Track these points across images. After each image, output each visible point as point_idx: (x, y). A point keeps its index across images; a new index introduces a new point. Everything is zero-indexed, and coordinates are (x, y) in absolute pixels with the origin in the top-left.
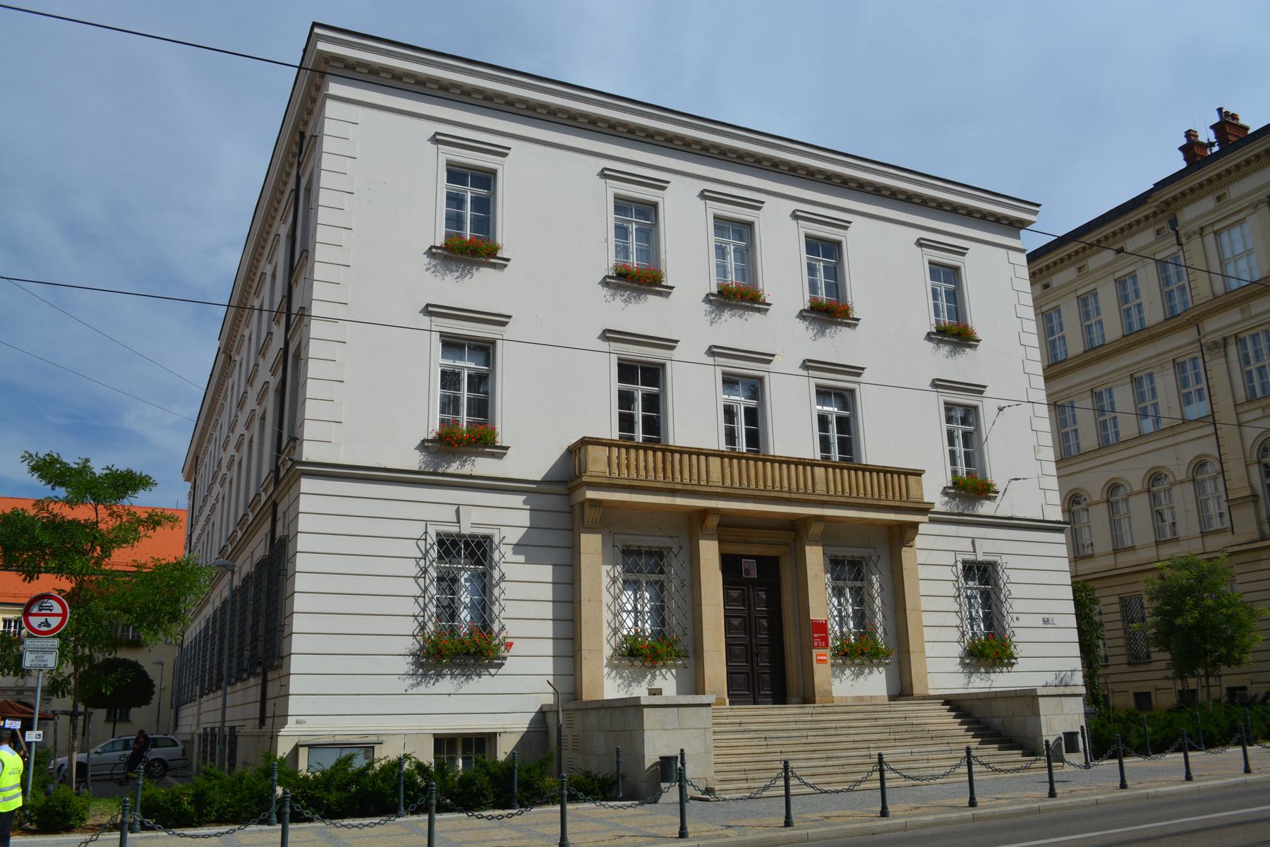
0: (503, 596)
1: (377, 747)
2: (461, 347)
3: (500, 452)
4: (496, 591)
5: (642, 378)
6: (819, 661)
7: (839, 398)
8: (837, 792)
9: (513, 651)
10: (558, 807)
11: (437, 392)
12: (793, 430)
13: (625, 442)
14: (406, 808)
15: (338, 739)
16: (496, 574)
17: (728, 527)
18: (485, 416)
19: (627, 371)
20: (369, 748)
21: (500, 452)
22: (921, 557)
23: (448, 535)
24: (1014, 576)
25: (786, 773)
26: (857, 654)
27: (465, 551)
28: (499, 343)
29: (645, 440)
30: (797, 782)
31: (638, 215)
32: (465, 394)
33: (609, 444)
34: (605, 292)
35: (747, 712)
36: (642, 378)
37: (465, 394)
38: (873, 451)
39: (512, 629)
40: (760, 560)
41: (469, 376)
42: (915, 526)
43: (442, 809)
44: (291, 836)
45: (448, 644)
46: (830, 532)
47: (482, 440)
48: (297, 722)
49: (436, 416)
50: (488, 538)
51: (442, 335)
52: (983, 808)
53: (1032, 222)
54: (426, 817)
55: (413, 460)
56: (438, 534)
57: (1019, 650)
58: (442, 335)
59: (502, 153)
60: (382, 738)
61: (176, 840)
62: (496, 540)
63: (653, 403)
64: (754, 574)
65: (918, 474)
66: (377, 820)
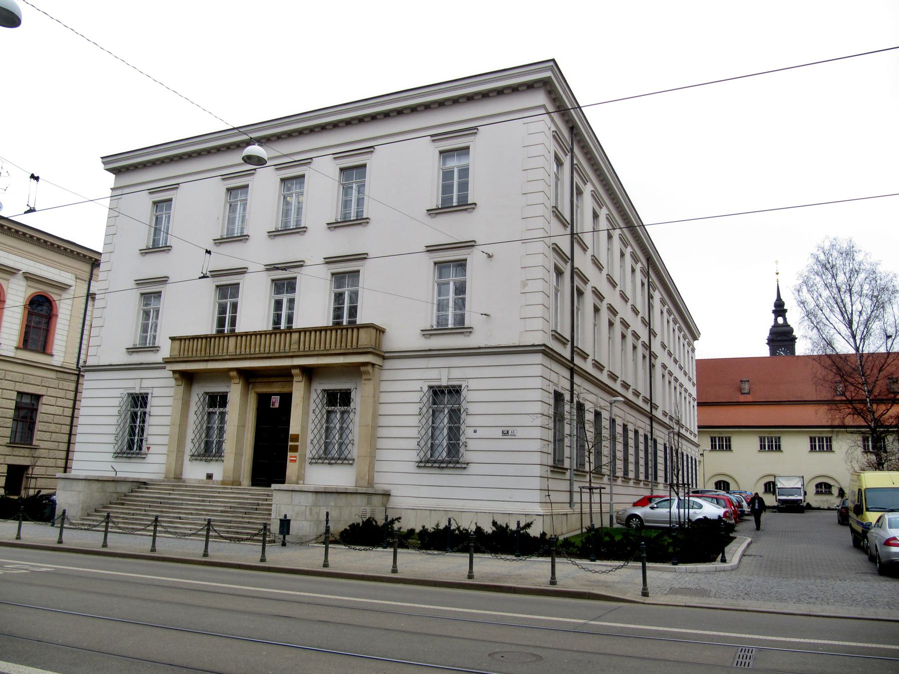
9: (151, 451)
34: (329, 232)
40: (281, 395)
64: (277, 405)
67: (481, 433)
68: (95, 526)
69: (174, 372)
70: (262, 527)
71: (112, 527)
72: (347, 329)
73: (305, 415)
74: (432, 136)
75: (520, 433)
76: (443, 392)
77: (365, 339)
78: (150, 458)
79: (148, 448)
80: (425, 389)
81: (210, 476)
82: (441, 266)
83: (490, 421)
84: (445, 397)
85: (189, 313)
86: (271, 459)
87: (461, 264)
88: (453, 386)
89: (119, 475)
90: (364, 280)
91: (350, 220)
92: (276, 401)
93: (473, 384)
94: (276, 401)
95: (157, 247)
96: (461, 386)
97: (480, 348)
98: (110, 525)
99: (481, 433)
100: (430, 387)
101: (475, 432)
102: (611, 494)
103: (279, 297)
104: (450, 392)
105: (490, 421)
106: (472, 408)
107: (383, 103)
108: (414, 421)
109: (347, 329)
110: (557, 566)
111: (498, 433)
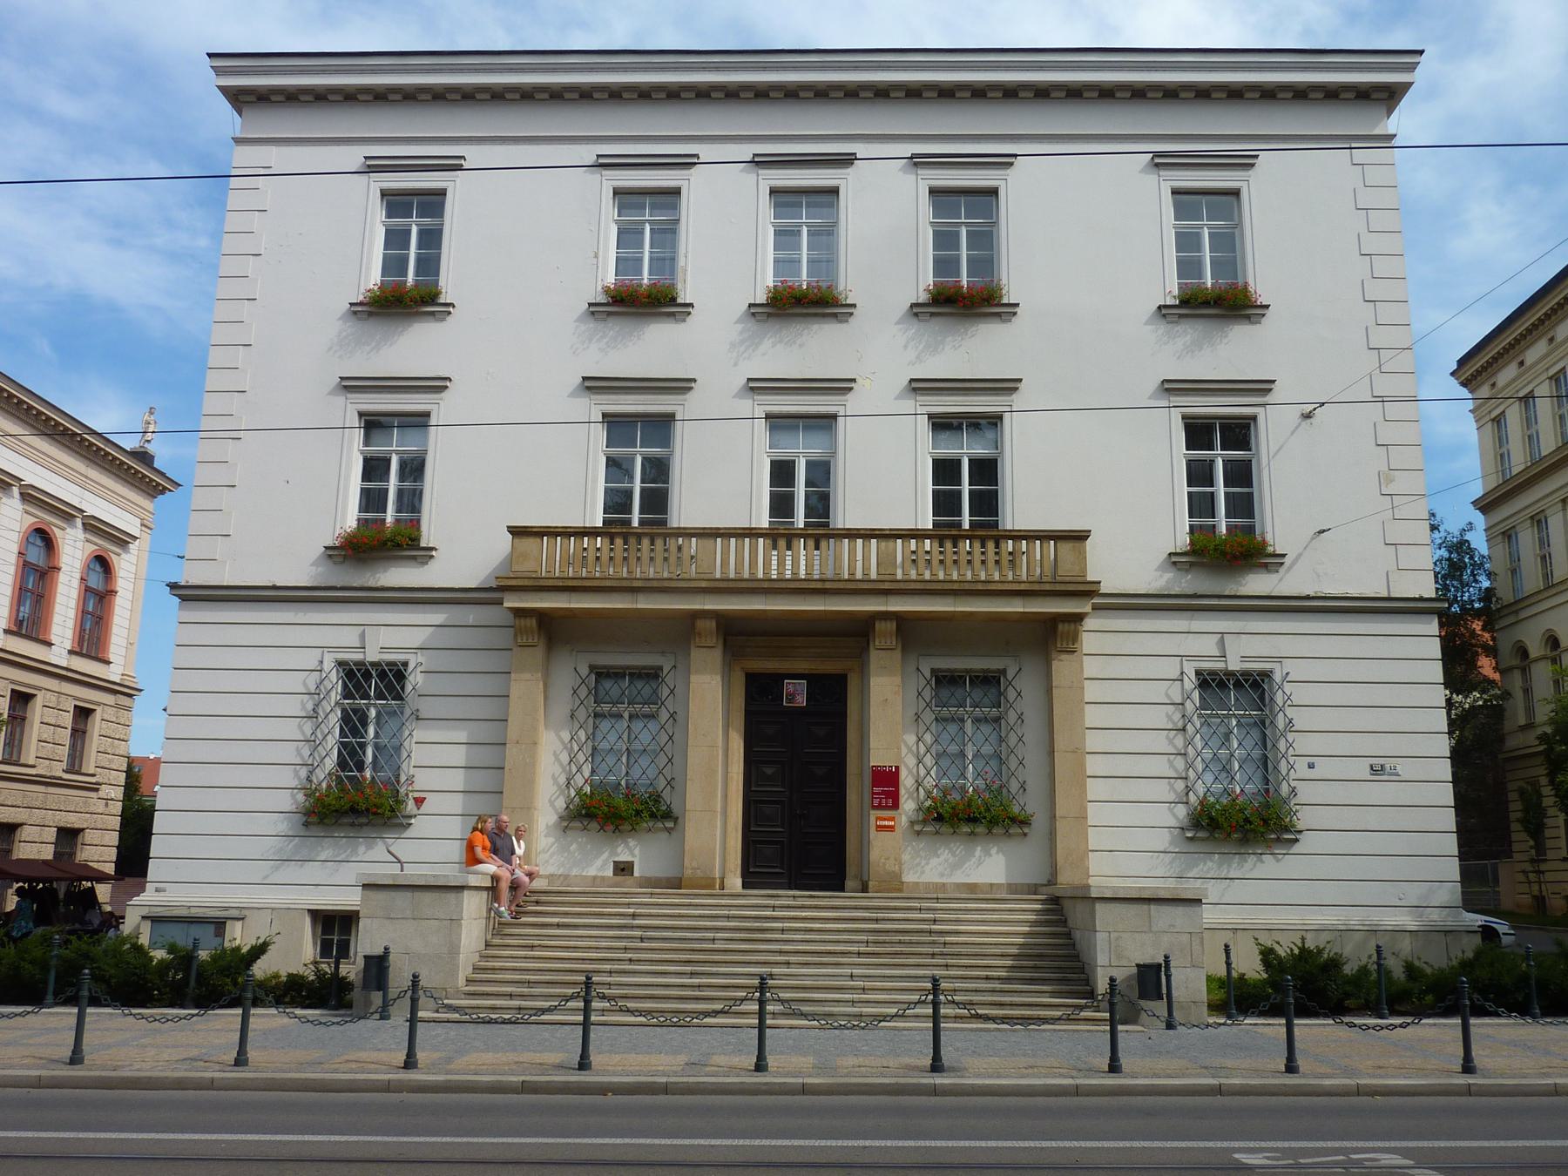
0: (1291, 751)
1: (229, 923)
2: (960, 427)
3: (424, 555)
4: (1282, 745)
5: (641, 431)
6: (880, 828)
7: (968, 428)
8: (504, 1022)
9: (425, 808)
10: (75, 1010)
11: (1183, 489)
12: (886, 479)
13: (945, 532)
14: (56, 995)
15: (194, 912)
16: (1281, 722)
17: (736, 635)
18: (1251, 515)
19: (1198, 432)
20: (219, 925)
21: (424, 555)
22: (1091, 667)
23: (1213, 673)
24: (1299, 694)
25: (588, 993)
26: (958, 817)
27: (372, 684)
28: (1007, 416)
29: (642, 522)
30: (778, 1008)
31: (650, 207)
32: (1220, 489)
33: (918, 535)
34: (1162, 327)
35: (758, 897)
36: (641, 431)
37: (1220, 489)
38: (1021, 508)
39: (423, 780)
40: (814, 680)
41: (808, 463)
42: (1079, 618)
43: (95, 1002)
44: (254, 1023)
45: (946, 810)
46: (913, 634)
47: (404, 543)
48: (157, 890)
49: (1185, 522)
50: (1266, 675)
51: (931, 416)
52: (1305, 1076)
53: (1406, 86)
54: (239, 1011)
55: (300, 570)
56: (1198, 673)
57: (1304, 818)
58: (931, 416)
59: (847, 160)
60: (245, 912)
61: (1354, 1034)
62: (1277, 677)
63: (1241, 474)
64: (801, 701)
65: (1080, 537)
66: (20, 1009)
67: (1324, 768)
68: (544, 1011)
69: (519, 613)
70: (756, 982)
71: (603, 1011)
72: (639, 536)
73: (894, 727)
74: (1157, 154)
75: (1405, 769)
76: (1222, 685)
77: (1034, 562)
78: (420, 825)
79: (419, 802)
80: (329, 664)
81: (623, 869)
82: (617, 425)
83: (1343, 744)
84: (1238, 692)
85: (512, 474)
86: (803, 826)
87: (661, 426)
88: (391, 664)
89: (409, 870)
90: (684, 435)
91: (964, 300)
92: (797, 694)
93: (1297, 670)
94: (797, 694)
95: (642, 301)
96: (405, 664)
97: (1308, 598)
98: (595, 1005)
99: (1324, 768)
100: (340, 664)
101: (1311, 766)
102: (1540, 883)
103: (783, 453)
104: (1238, 685)
105: (1343, 744)
106: (1301, 719)
107: (856, 67)
108: (1093, 741)
109: (639, 536)
110: (1296, 1031)
111: (1361, 769)
